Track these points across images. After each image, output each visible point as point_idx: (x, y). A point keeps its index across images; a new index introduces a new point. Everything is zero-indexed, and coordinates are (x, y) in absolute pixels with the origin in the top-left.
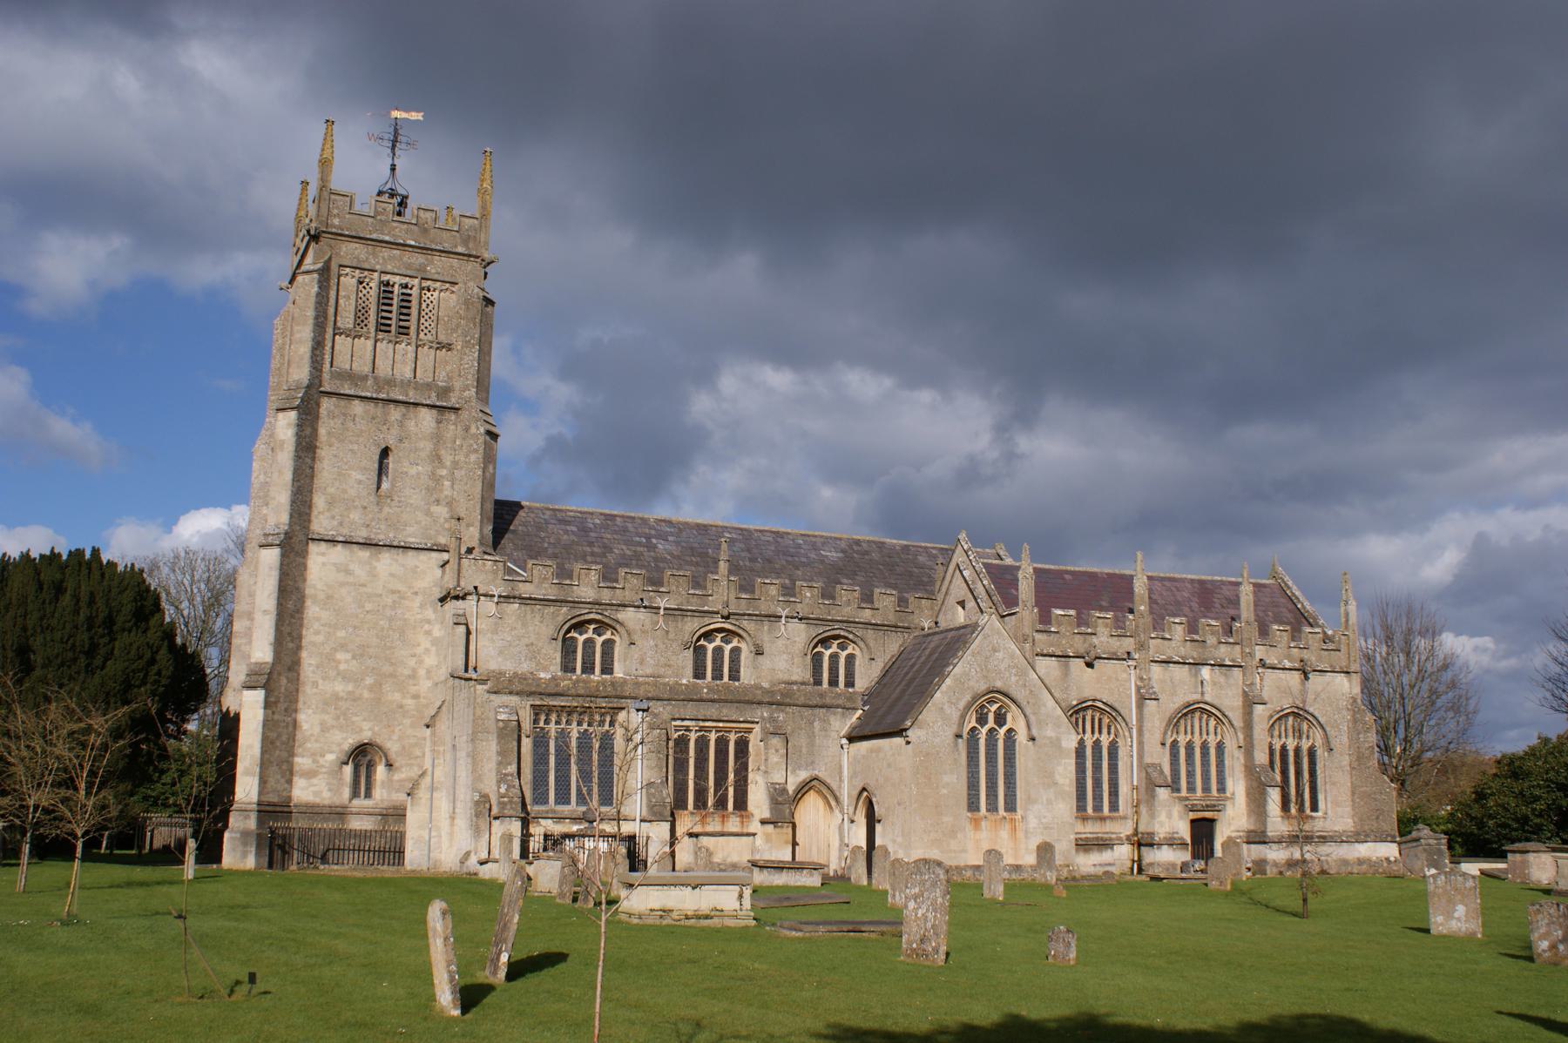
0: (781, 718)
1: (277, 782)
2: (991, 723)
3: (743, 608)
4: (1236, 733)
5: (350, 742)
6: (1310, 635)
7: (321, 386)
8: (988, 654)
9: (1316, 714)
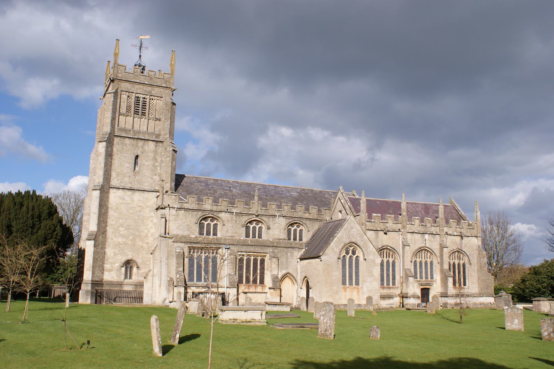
0: (276, 252)
1: (98, 273)
2: (350, 254)
3: (263, 212)
5: (124, 259)
7: (114, 133)
9: (465, 251)
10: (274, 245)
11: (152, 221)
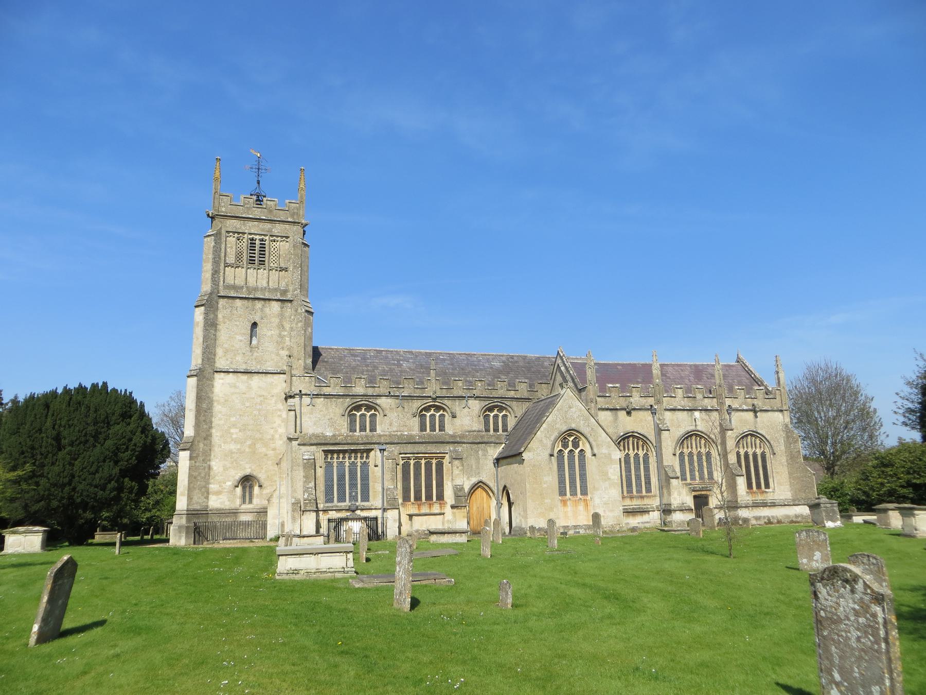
0: (460, 450)
1: (199, 498)
2: (570, 447)
3: (444, 393)
4: (717, 447)
5: (239, 475)
6: (758, 391)
8: (567, 409)
9: (764, 434)
11: (280, 416)
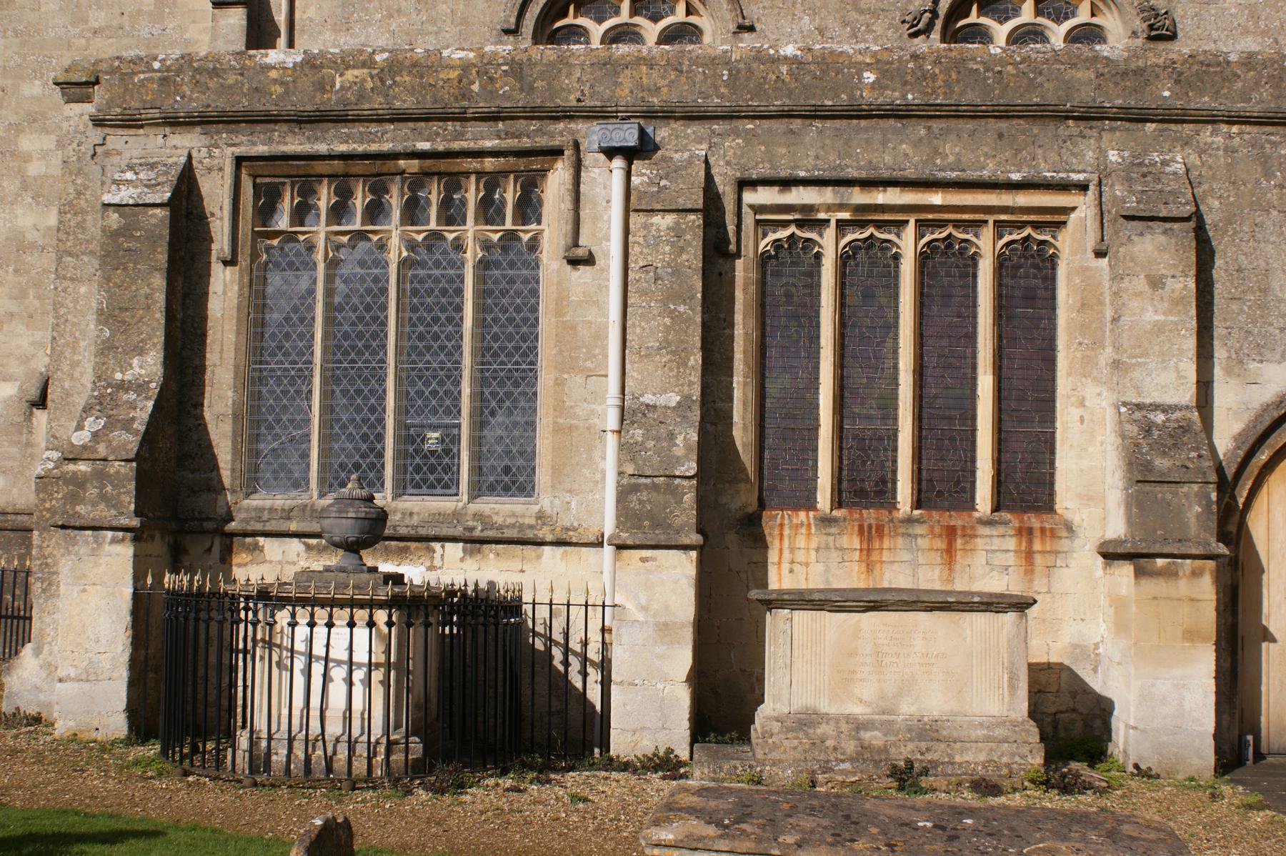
10: (1147, 101)
